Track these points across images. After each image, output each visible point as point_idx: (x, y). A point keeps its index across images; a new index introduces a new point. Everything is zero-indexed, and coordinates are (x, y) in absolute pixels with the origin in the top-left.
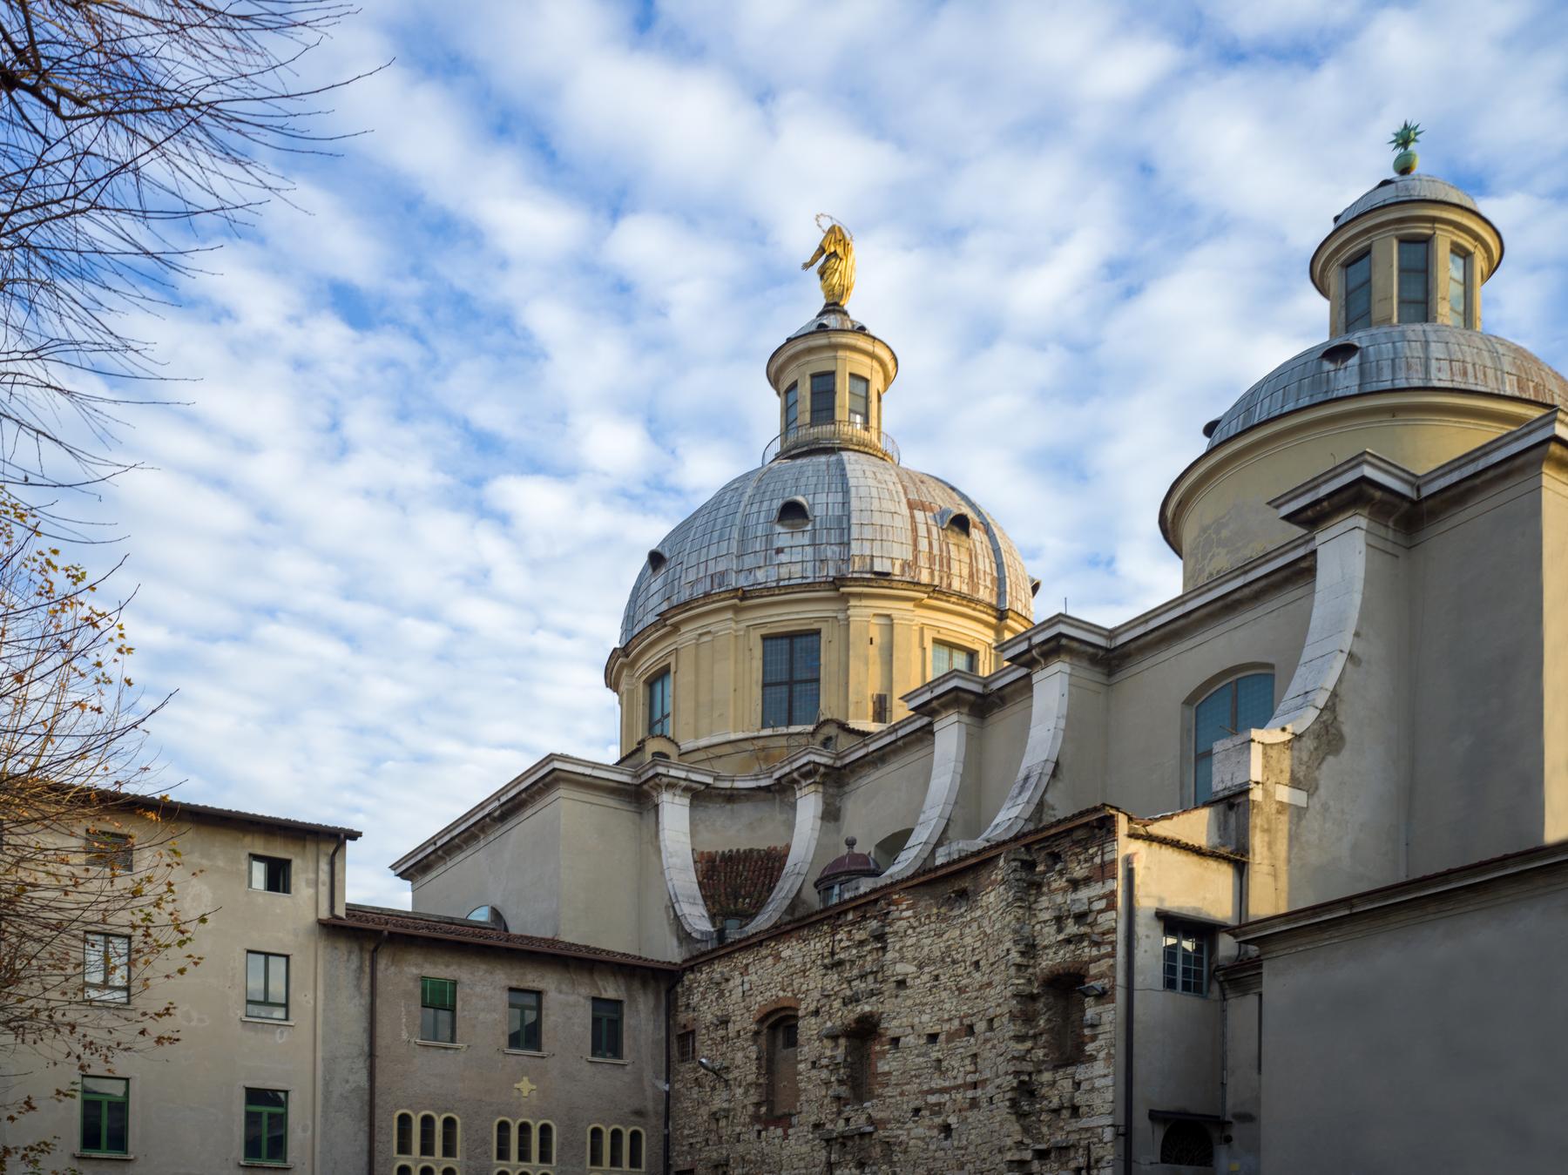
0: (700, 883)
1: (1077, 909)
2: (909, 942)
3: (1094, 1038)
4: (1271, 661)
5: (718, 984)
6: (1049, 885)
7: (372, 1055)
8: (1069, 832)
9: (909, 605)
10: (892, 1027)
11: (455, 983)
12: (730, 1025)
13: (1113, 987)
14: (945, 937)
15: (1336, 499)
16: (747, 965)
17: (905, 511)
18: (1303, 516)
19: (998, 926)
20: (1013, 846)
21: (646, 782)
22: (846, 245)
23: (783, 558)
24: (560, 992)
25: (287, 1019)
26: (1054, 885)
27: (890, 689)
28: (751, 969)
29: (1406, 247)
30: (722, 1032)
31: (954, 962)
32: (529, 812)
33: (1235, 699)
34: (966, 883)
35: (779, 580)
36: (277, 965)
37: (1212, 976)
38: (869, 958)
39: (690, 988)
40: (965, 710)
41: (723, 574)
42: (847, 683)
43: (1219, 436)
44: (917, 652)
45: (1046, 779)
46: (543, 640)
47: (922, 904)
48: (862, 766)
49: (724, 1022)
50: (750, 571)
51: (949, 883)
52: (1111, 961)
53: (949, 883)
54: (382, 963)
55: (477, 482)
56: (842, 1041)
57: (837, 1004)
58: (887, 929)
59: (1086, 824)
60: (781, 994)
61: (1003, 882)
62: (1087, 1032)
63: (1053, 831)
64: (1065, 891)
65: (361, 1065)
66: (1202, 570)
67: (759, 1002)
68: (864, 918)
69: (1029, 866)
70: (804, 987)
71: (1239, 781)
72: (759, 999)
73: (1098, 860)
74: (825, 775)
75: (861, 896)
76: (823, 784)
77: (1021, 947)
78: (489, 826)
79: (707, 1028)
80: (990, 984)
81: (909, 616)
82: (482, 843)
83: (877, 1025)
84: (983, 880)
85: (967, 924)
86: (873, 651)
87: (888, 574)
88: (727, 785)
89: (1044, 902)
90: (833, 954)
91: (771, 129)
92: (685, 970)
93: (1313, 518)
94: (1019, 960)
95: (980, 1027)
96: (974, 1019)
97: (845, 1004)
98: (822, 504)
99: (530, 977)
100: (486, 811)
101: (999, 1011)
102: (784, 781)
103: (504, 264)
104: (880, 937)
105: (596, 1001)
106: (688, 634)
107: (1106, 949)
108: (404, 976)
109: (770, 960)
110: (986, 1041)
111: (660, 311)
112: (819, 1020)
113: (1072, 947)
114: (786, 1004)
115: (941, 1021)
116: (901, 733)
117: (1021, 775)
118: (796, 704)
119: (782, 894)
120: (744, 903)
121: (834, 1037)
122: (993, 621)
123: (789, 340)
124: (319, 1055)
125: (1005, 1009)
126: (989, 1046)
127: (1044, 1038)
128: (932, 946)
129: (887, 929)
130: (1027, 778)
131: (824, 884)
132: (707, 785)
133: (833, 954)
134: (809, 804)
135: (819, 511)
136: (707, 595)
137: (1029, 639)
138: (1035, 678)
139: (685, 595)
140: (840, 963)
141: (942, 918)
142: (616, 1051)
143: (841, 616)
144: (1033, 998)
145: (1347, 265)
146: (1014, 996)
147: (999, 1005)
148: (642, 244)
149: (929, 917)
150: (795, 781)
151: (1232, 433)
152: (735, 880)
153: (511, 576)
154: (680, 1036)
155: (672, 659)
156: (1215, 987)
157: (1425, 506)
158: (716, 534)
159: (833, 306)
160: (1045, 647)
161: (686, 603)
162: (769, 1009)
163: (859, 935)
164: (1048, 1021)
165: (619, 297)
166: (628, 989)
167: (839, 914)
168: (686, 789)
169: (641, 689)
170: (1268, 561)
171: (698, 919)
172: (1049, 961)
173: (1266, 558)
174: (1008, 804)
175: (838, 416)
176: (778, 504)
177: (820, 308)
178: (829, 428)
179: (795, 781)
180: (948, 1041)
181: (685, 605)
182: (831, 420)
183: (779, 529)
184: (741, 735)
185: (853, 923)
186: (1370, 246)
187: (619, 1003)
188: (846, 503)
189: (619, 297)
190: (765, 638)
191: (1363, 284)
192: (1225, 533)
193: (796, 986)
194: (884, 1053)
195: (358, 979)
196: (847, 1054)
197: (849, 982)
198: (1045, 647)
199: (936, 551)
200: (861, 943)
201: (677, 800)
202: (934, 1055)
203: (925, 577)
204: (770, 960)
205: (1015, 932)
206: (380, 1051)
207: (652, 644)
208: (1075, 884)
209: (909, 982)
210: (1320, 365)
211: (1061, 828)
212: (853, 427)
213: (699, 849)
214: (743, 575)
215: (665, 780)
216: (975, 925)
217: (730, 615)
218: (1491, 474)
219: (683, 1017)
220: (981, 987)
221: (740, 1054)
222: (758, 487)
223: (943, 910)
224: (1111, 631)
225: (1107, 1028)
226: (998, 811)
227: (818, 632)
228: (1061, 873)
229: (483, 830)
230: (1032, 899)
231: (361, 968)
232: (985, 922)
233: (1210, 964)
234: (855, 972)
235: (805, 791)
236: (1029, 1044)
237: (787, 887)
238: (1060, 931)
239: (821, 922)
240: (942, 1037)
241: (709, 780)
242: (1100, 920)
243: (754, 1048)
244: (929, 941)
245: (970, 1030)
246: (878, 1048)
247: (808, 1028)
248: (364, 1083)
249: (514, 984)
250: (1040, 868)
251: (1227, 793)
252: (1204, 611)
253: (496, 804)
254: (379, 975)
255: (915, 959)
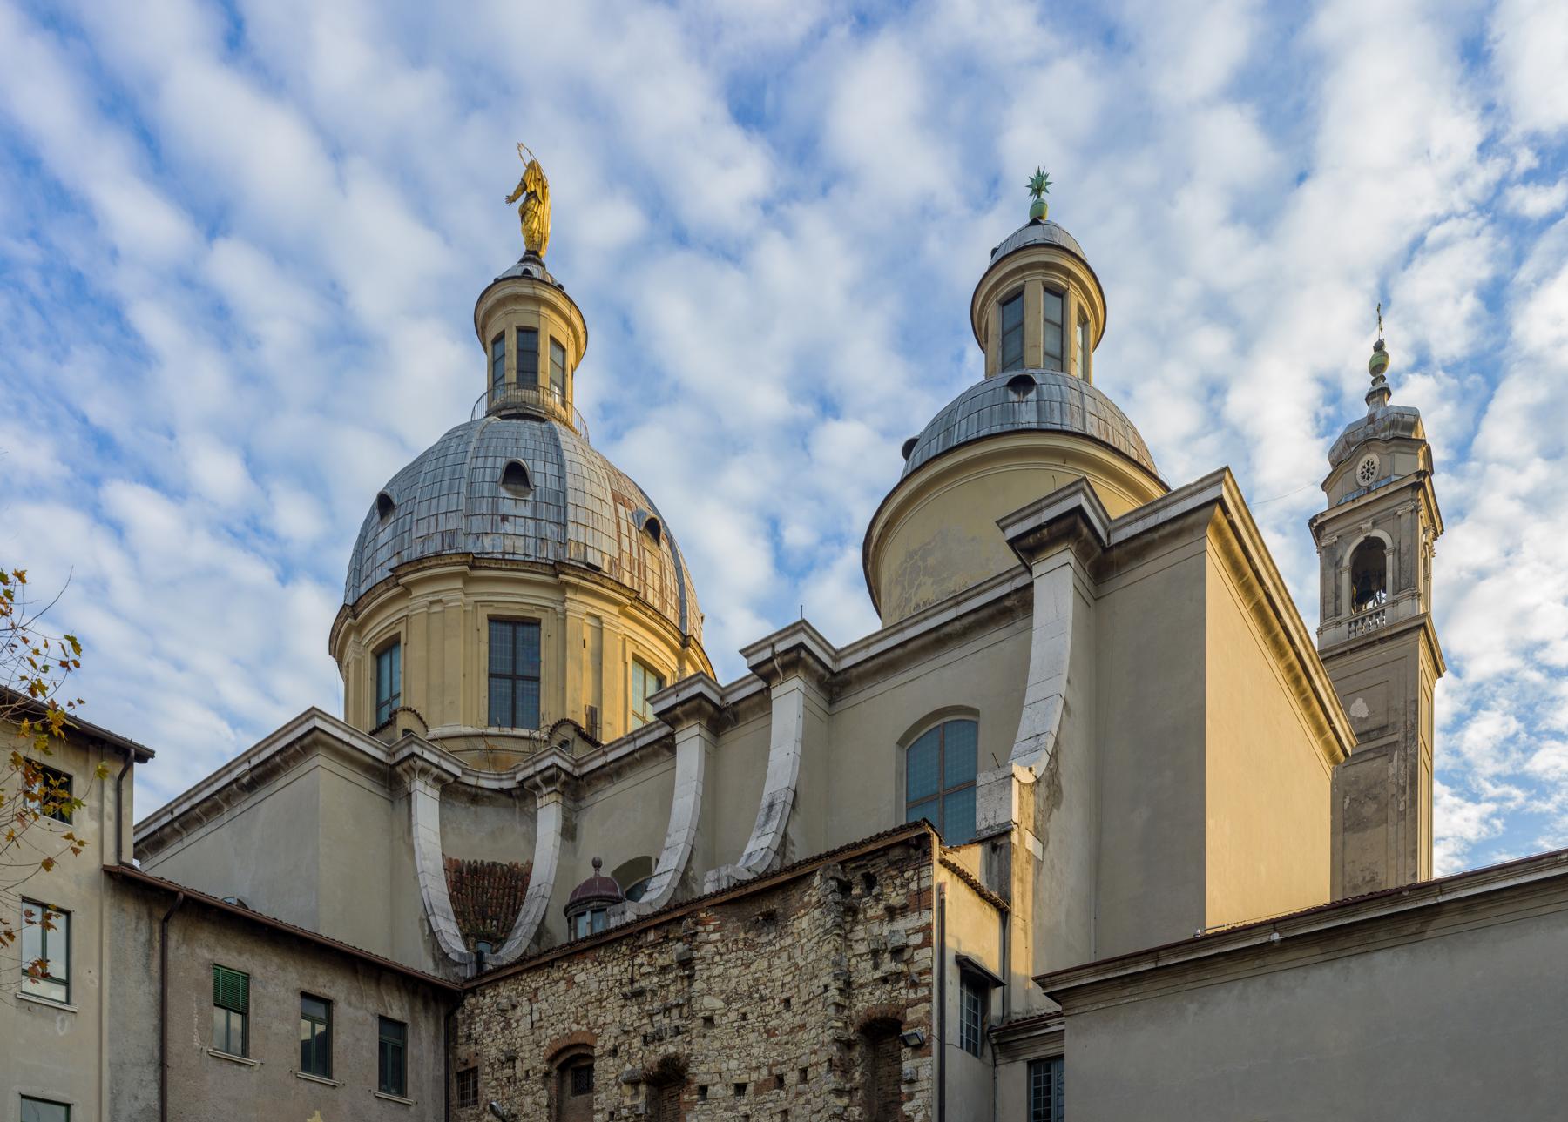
0: (451, 896)
1: (898, 941)
2: (718, 970)
3: (911, 1097)
4: (977, 706)
5: (504, 1011)
6: (865, 911)
7: (163, 1065)
8: (886, 849)
9: (615, 610)
10: (700, 1073)
11: (247, 977)
12: (518, 1063)
13: (930, 1037)
14: (753, 968)
15: (1054, 528)
16: (536, 990)
17: (611, 502)
18: (1025, 543)
19: (812, 957)
20: (831, 862)
21: (400, 762)
22: (544, 187)
23: (508, 527)
24: (350, 1004)
25: (68, 1002)
26: (871, 913)
27: (601, 704)
28: (541, 995)
29: (494, 626)
30: (508, 1072)
31: (762, 999)
32: (281, 782)
33: (942, 743)
34: (775, 905)
35: (504, 553)
36: (59, 922)
37: (985, 1037)
38: (672, 988)
39: (471, 1015)
40: (704, 723)
41: (453, 533)
42: (564, 688)
43: (918, 457)
44: (621, 664)
45: (788, 808)
46: (157, 668)
47: (730, 926)
48: (599, 778)
49: (512, 1059)
50: (478, 535)
51: (760, 901)
52: (927, 1006)
53: (760, 901)
54: (174, 938)
55: (95, 481)
56: (643, 1088)
57: (637, 1042)
58: (695, 954)
59: (905, 843)
60: (575, 1027)
61: (820, 904)
62: (904, 1088)
63: (871, 848)
64: (880, 919)
65: (151, 1075)
66: (908, 600)
67: (551, 1036)
68: (666, 939)
69: (845, 888)
70: (601, 1020)
71: (1001, 820)
72: (550, 1032)
73: (914, 886)
74: (565, 784)
75: (628, 925)
76: (562, 794)
77: (840, 984)
78: (236, 795)
79: (492, 1065)
80: (802, 1027)
81: (619, 625)
82: (226, 817)
83: (684, 1068)
84: (794, 902)
85: (776, 954)
86: (586, 655)
87: (599, 569)
88: (472, 781)
89: (860, 932)
90: (632, 981)
91: (340, 183)
92: (466, 992)
93: (1029, 547)
94: (838, 999)
95: (792, 1077)
96: (784, 1068)
97: (646, 1042)
98: (540, 472)
99: (321, 980)
100: (234, 775)
101: (814, 1059)
102: (526, 785)
103: (114, 254)
104: (686, 963)
105: (384, 1020)
106: (420, 599)
107: (922, 992)
108: (200, 955)
109: (562, 985)
110: (799, 1095)
111: (253, 343)
112: (617, 1061)
113: (888, 987)
114: (580, 1040)
115: (749, 1068)
116: (639, 743)
117: (765, 802)
118: (519, 703)
119: (529, 919)
120: (491, 926)
121: (634, 1083)
122: (678, 646)
123: (497, 281)
124: (105, 1057)
125: (823, 1057)
126: (802, 1100)
127: (860, 1093)
128: (739, 979)
129: (695, 954)
130: (771, 806)
131: (574, 910)
132: (456, 777)
133: (632, 981)
134: (549, 815)
135: (537, 481)
136: (438, 555)
137: (773, 646)
138: (775, 693)
139: (416, 552)
140: (640, 993)
141: (749, 945)
142: (401, 1089)
143: (559, 608)
144: (848, 1045)
145: (1004, 303)
146: (835, 1040)
147: (814, 1052)
148: (235, 268)
149: (736, 942)
150: (537, 787)
151: (933, 453)
152: (485, 893)
153: (126, 593)
154: (460, 1075)
155: (401, 628)
156: (988, 1050)
157: (1115, 553)
158: (446, 484)
159: (532, 256)
160: (787, 658)
161: (420, 560)
162: (562, 1045)
163: (661, 961)
164: (862, 1074)
165: (218, 319)
166: (412, 1010)
167: (640, 932)
168: (437, 779)
169: (369, 660)
170: (978, 594)
171: (453, 940)
172: (868, 1001)
173: (977, 590)
174: (756, 833)
175: (541, 383)
176: (501, 463)
177: (521, 255)
178: (532, 394)
179: (537, 787)
180: (757, 1092)
181: (418, 563)
182: (535, 386)
183: (503, 492)
184: (469, 730)
185: (654, 945)
186: (1023, 286)
187: (402, 1025)
188: (561, 478)
189: (218, 319)
190: (493, 620)
191: (1016, 327)
192: (931, 561)
193: (591, 1018)
194: (692, 1103)
195: (148, 956)
196: (648, 1104)
197: (651, 1016)
198: (787, 658)
199: (635, 555)
200: (664, 970)
201: (429, 790)
202: (743, 1110)
203: (626, 581)
204: (562, 985)
205: (836, 964)
206: (171, 1060)
207: (381, 607)
208: (892, 913)
209: (717, 1020)
210: (1006, 394)
211: (880, 845)
212: (554, 401)
213: (449, 855)
214: (472, 538)
215: (420, 763)
216: (784, 956)
217: (459, 584)
218: (1168, 529)
219: (464, 1051)
220: (792, 1030)
221: (529, 1100)
222: (481, 440)
223: (750, 935)
224: (837, 652)
225: (925, 1085)
226: (745, 845)
227: (537, 623)
228: (877, 899)
229: (227, 800)
230: (848, 927)
231: (150, 941)
232: (797, 953)
233: (983, 1024)
234: (657, 1004)
235: (546, 800)
236: (846, 1100)
237: (533, 911)
238: (876, 967)
239: (619, 940)
240: (750, 1089)
241: (458, 772)
242: (916, 958)
243: (545, 1092)
244: (735, 972)
245: (780, 1081)
246: (686, 1097)
247: (605, 1070)
248: (155, 1104)
249: (306, 988)
250: (856, 891)
251: (990, 832)
252: (972, 618)
253: (246, 767)
254: (170, 956)
255: (722, 992)
